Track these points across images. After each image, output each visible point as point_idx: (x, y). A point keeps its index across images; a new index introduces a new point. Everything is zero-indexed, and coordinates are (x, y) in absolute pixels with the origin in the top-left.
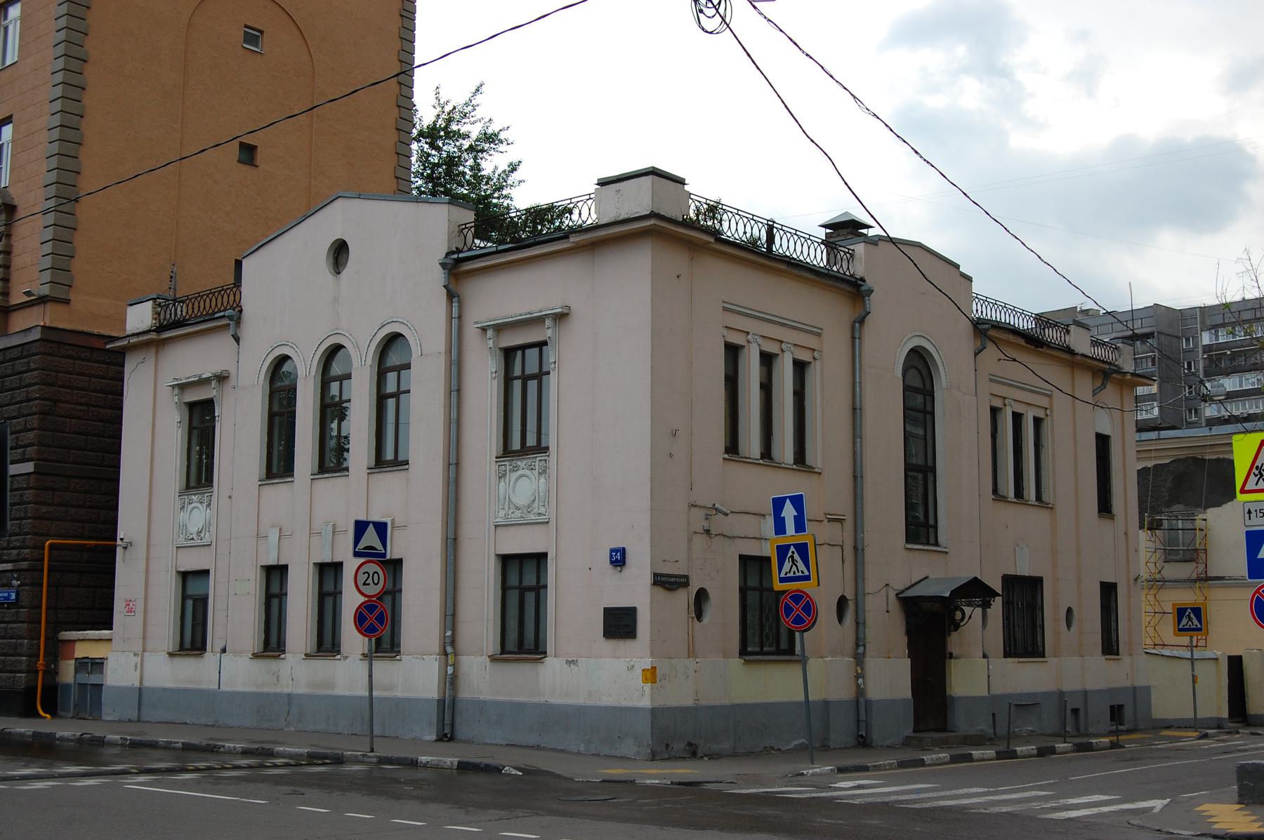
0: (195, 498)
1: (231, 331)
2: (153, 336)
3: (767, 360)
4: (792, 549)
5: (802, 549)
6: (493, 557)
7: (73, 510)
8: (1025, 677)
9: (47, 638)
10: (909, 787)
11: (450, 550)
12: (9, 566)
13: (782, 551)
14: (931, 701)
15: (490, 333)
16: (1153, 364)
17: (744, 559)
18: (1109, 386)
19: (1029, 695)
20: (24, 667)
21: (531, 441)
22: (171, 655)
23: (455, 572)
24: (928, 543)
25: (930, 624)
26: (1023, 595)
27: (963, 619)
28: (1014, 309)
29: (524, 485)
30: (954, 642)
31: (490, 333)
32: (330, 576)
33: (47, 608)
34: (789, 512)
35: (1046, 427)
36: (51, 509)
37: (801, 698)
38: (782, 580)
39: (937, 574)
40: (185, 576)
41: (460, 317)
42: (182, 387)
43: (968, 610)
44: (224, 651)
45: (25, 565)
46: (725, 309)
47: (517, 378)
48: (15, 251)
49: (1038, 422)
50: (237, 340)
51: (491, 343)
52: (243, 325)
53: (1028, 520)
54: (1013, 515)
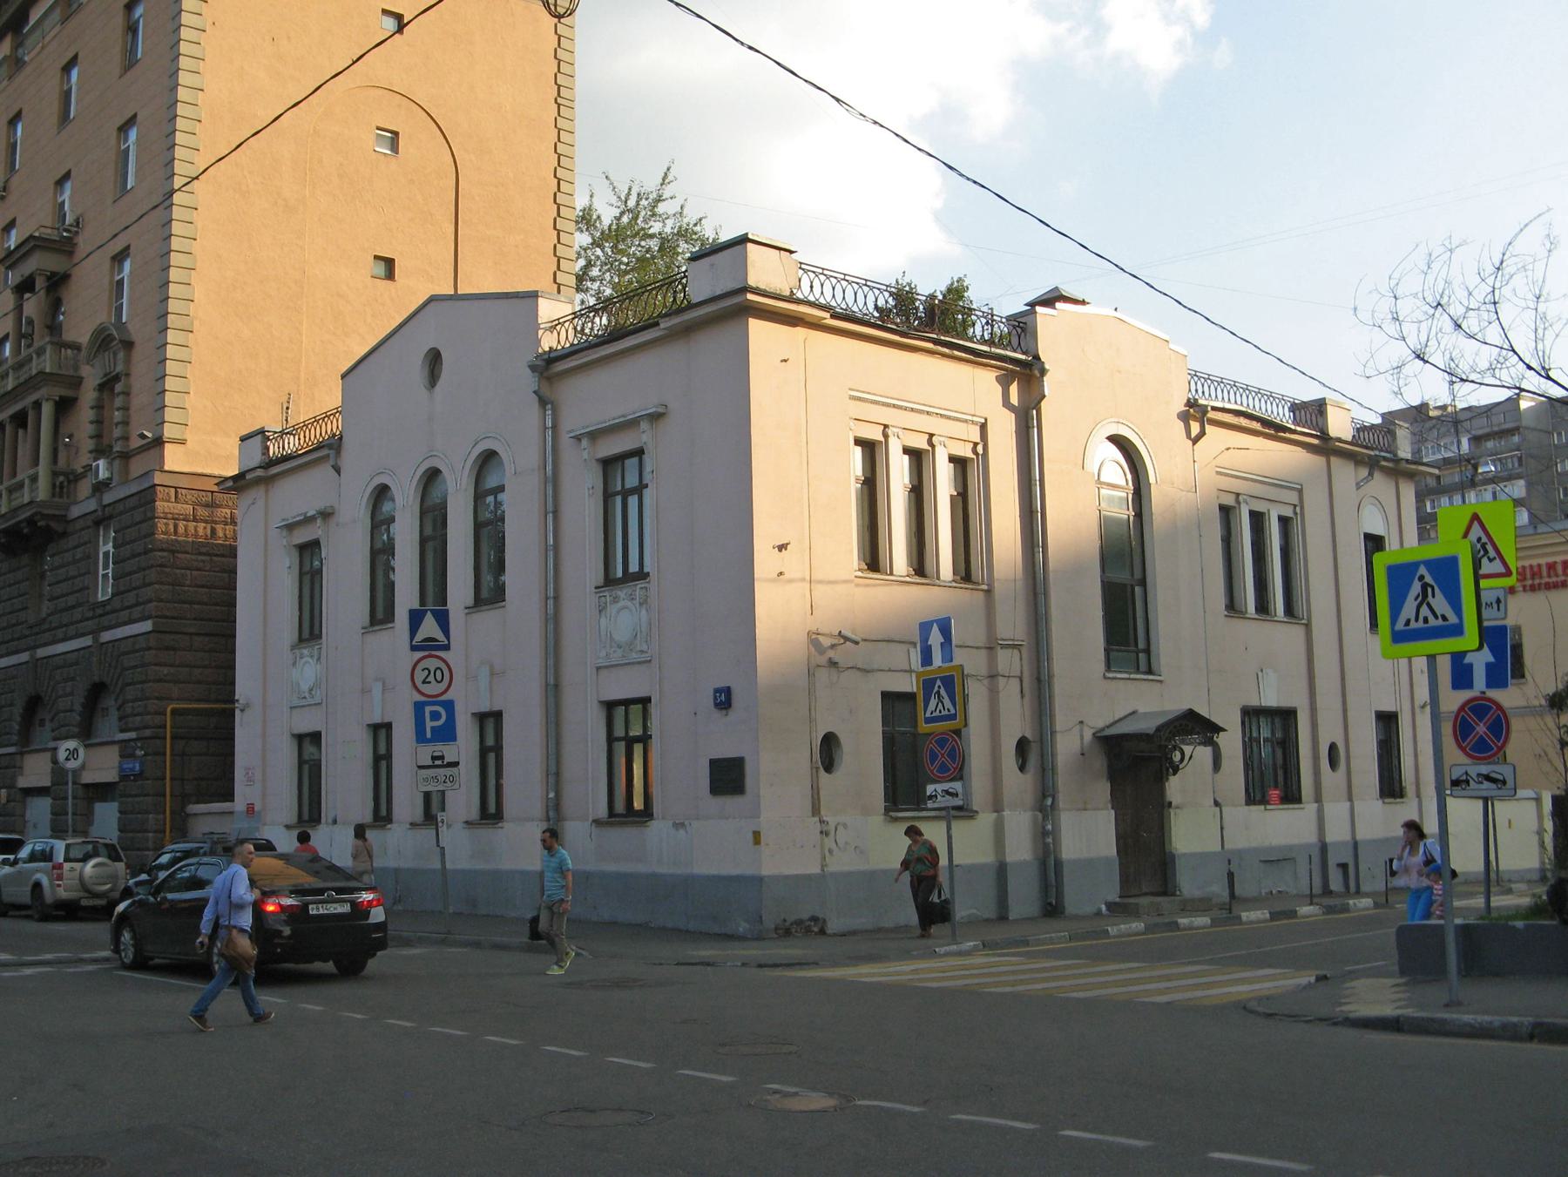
0: (305, 652)
1: (332, 462)
2: (260, 472)
3: (917, 457)
4: (939, 683)
5: (948, 682)
6: (596, 705)
7: (197, 671)
8: (1282, 826)
9: (172, 812)
10: (1122, 966)
11: (551, 700)
12: (133, 735)
13: (928, 685)
14: (1146, 855)
15: (585, 442)
16: (1520, 465)
17: (886, 696)
18: (1377, 475)
19: (1280, 849)
20: (150, 845)
21: (634, 567)
22: (597, 822)
23: (558, 725)
24: (1138, 671)
25: (1138, 765)
26: (1274, 729)
27: (1182, 759)
28: (1271, 395)
29: (626, 617)
30: (1175, 787)
31: (585, 442)
32: (382, 734)
33: (172, 779)
34: (936, 638)
35: (1296, 529)
36: (172, 670)
37: (1348, 837)
38: (928, 721)
39: (1142, 703)
40: (300, 738)
41: (554, 427)
42: (290, 527)
43: (1188, 749)
44: (335, 822)
45: (148, 733)
46: (853, 398)
47: (618, 493)
48: (135, 390)
49: (1284, 521)
50: (338, 470)
51: (585, 455)
52: (344, 454)
53: (1282, 638)
54: (1253, 631)
